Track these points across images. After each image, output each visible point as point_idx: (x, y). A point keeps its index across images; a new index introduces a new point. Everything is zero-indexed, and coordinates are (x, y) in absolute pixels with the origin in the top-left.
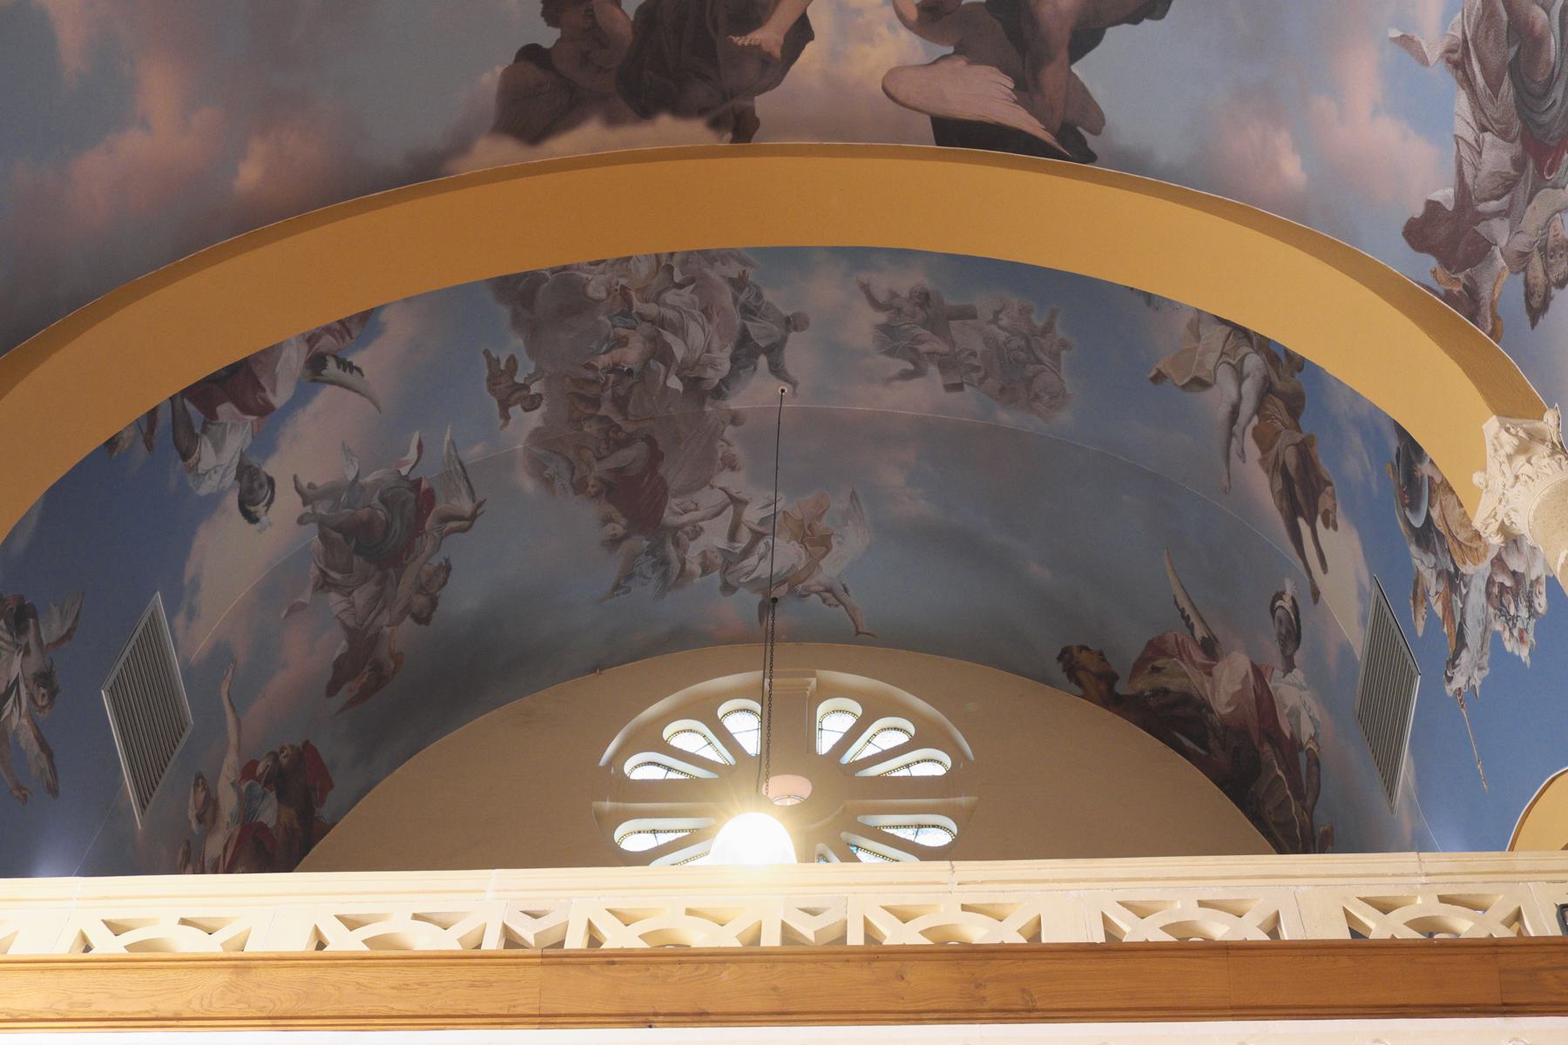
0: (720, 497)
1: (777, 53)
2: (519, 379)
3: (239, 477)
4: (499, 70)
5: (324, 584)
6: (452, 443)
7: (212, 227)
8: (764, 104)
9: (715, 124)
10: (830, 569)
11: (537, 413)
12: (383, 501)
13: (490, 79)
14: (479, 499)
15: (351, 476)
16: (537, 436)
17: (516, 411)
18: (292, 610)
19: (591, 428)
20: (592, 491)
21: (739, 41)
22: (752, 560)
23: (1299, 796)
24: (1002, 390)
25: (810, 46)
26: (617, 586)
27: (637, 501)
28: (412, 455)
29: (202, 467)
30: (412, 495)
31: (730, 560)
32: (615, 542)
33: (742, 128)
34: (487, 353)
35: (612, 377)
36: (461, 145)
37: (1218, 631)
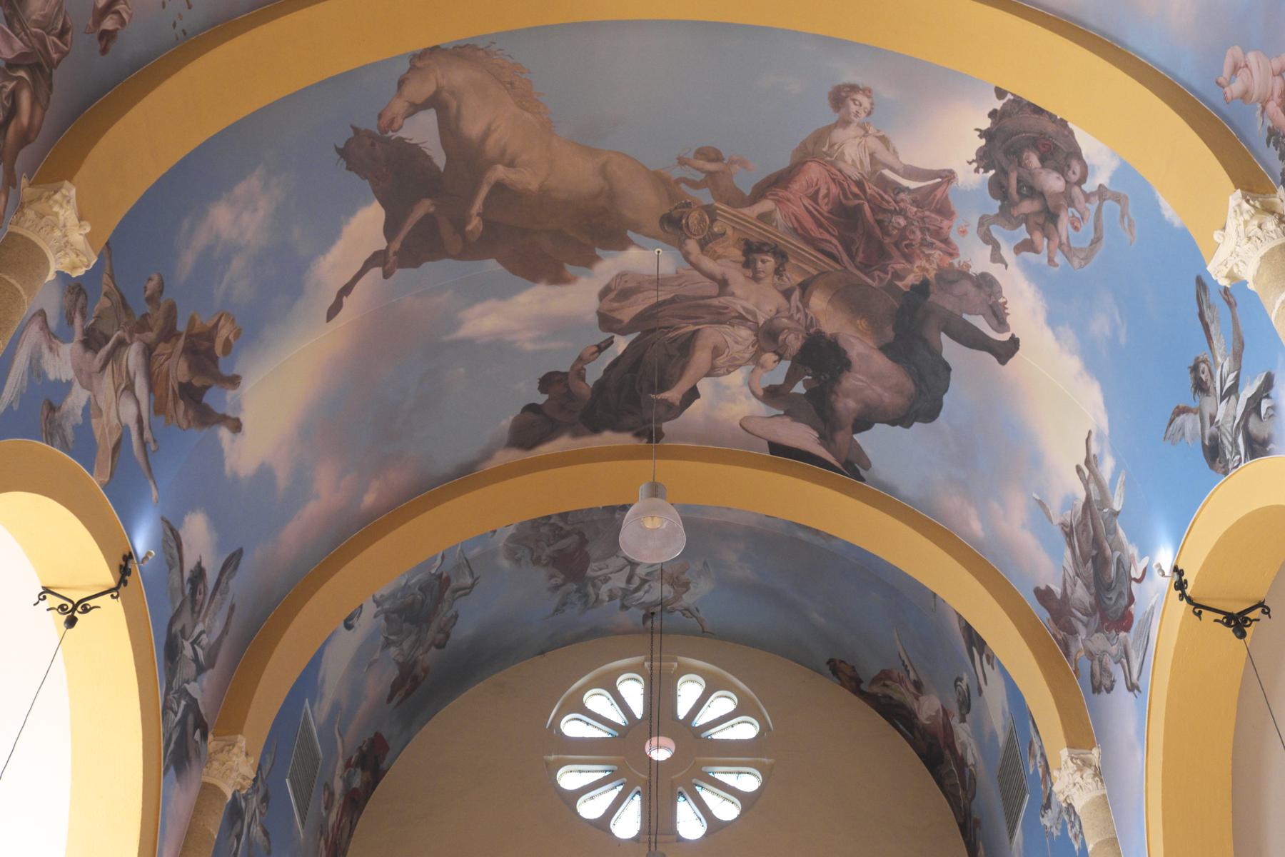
1: (678, 403)
4: (511, 418)
5: (388, 644)
8: (666, 427)
9: (638, 435)
10: (687, 600)
12: (420, 589)
13: (506, 423)
18: (369, 666)
22: (641, 593)
23: (964, 788)
25: (697, 402)
26: (557, 610)
31: (626, 593)
32: (557, 587)
33: (651, 435)
36: (488, 455)
37: (924, 681)
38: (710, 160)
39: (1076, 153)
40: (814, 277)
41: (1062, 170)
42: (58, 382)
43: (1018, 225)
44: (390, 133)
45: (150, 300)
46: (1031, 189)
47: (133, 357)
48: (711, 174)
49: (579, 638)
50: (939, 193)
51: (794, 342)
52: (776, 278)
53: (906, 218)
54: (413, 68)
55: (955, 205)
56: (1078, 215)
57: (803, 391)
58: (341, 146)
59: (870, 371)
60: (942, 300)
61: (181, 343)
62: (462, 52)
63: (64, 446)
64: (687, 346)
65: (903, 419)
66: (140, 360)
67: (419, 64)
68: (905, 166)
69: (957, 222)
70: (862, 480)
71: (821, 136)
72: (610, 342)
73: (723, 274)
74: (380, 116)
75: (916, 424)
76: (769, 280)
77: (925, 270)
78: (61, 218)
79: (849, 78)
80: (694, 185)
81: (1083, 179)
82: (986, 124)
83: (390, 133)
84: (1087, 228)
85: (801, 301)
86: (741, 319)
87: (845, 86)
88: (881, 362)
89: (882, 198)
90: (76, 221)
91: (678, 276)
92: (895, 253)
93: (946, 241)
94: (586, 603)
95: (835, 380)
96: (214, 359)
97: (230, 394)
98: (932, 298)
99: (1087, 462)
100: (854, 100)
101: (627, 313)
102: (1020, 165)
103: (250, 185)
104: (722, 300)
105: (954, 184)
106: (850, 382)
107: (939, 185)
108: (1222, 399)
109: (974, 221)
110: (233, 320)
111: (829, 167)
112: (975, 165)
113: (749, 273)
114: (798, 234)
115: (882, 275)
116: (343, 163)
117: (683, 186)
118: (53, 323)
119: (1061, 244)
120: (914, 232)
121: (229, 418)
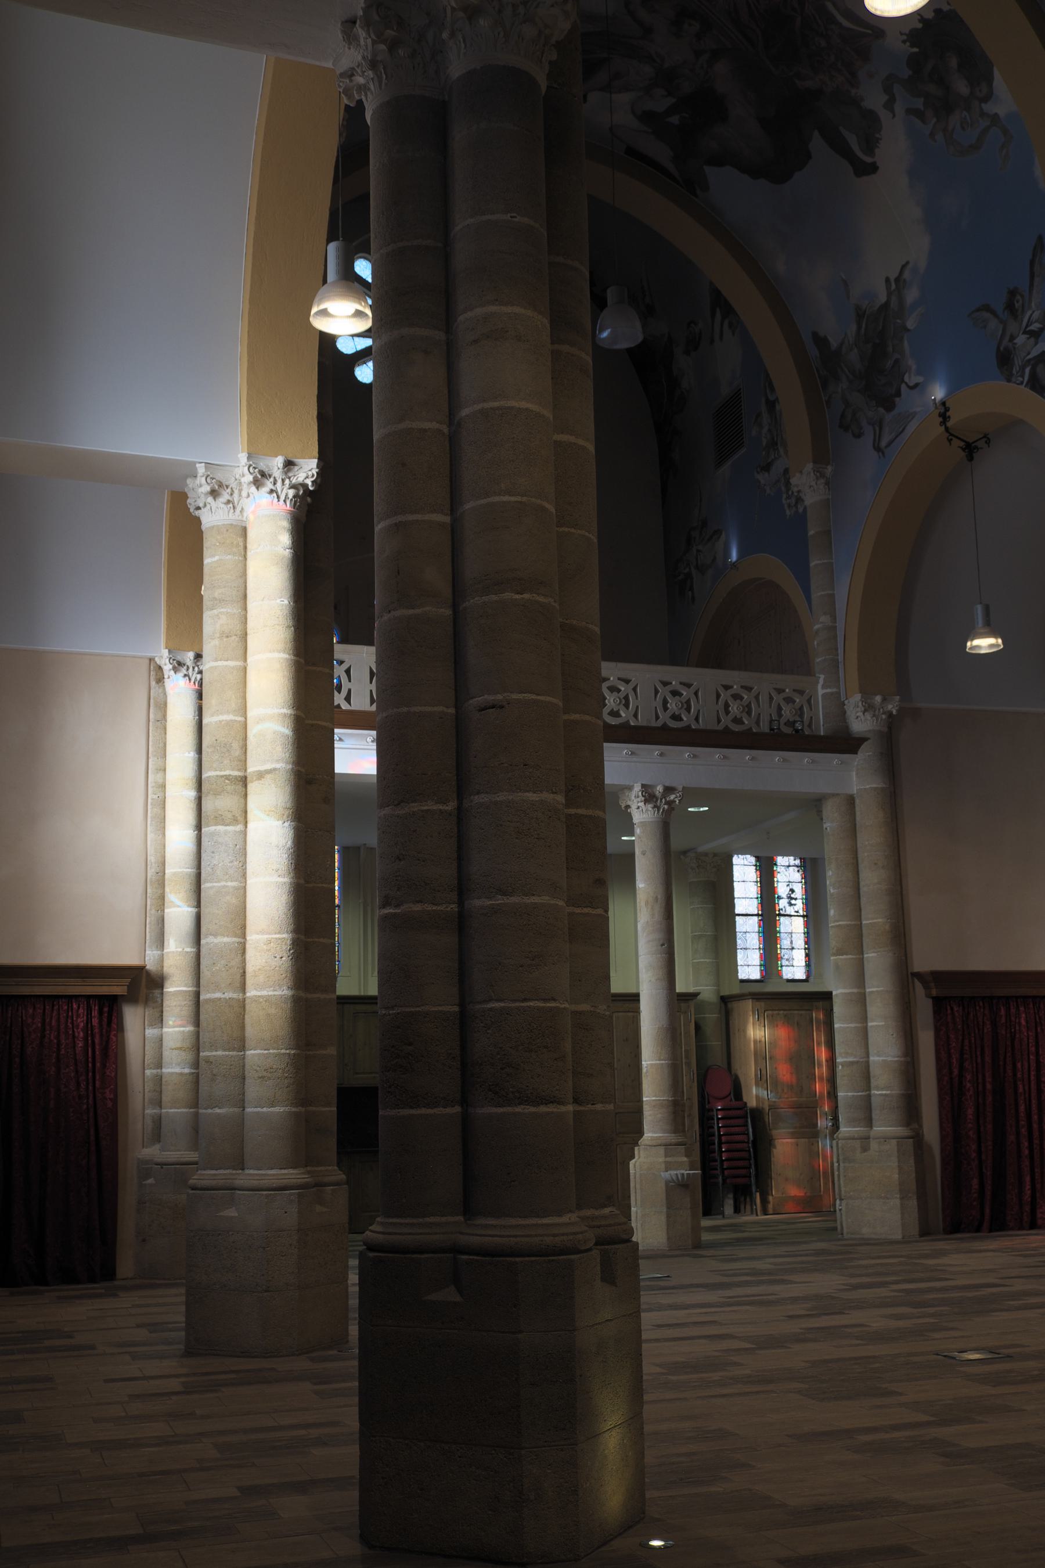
81: (986, 99)
99: (897, 280)
108: (1025, 332)
112: (905, 37)
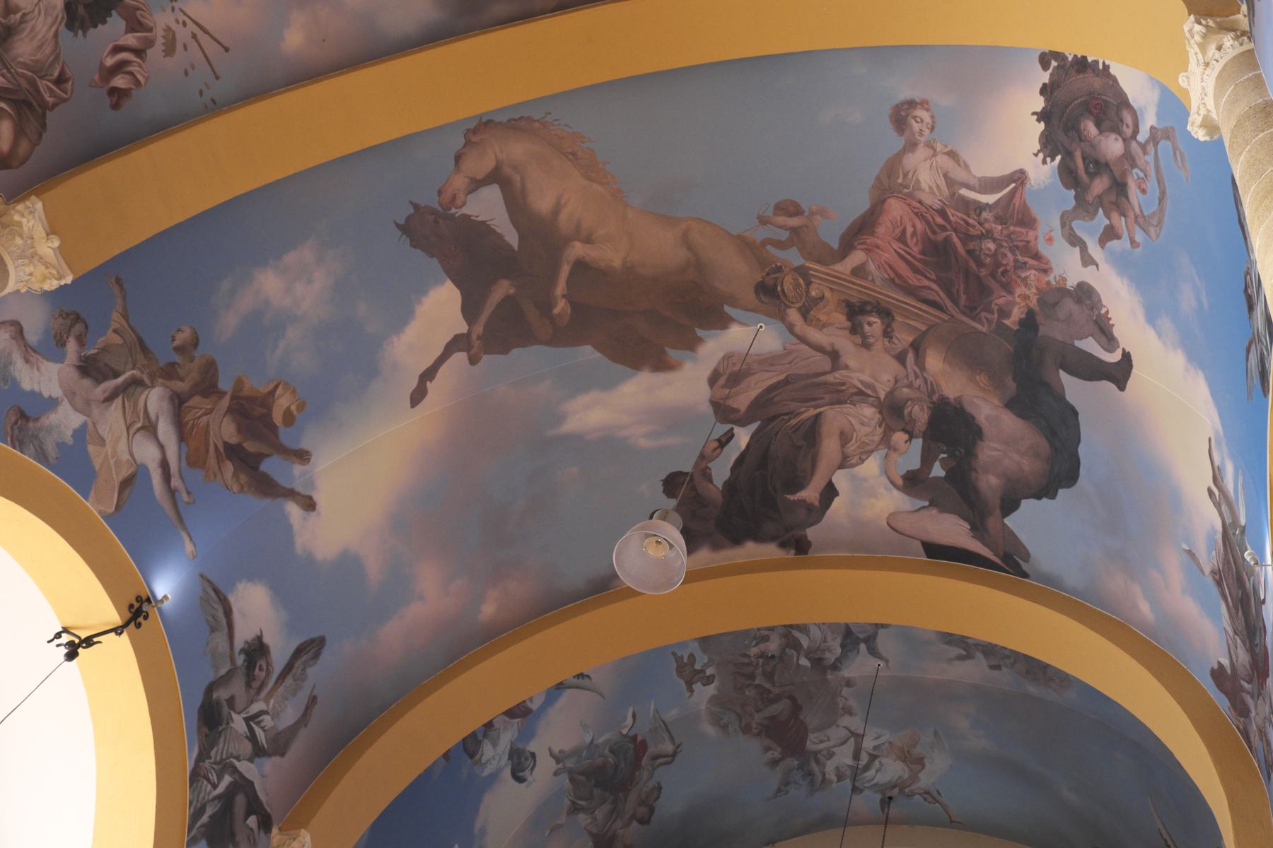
0: (844, 733)
1: (817, 503)
2: (698, 667)
3: (510, 757)
5: (575, 809)
6: (656, 711)
7: (464, 646)
8: (811, 533)
9: (783, 545)
10: (926, 780)
11: (712, 686)
12: (612, 751)
14: (678, 742)
15: (588, 739)
16: (714, 700)
17: (698, 687)
18: (552, 830)
19: (750, 693)
20: (755, 731)
21: (791, 497)
24: (1027, 672)
26: (779, 791)
27: (787, 736)
28: (629, 721)
29: (484, 759)
30: (632, 746)
31: (856, 773)
33: (801, 546)
34: (674, 654)
35: (761, 661)
38: (791, 215)
39: (1123, 102)
40: (924, 334)
41: (1116, 129)
42: (35, 396)
43: (1096, 212)
44: (453, 210)
45: (180, 350)
46: (1097, 162)
47: (155, 400)
48: (794, 230)
49: (807, 830)
50: (1017, 201)
51: (920, 414)
52: (886, 340)
53: (994, 240)
54: (468, 143)
55: (1036, 210)
56: (1141, 175)
57: (942, 473)
58: (402, 221)
59: (1005, 440)
60: (1051, 330)
61: (225, 402)
62: (516, 123)
63: (42, 456)
64: (812, 432)
65: (1046, 490)
66: (166, 405)
67: (474, 139)
68: (980, 179)
69: (1042, 230)
70: (1026, 575)
71: (893, 166)
72: (730, 436)
73: (832, 345)
74: (440, 193)
75: (1061, 492)
76: (879, 345)
77: (1026, 297)
78: (25, 229)
79: (905, 94)
80: (780, 245)
81: (1136, 131)
82: (1039, 104)
83: (453, 210)
84: (1152, 185)
85: (916, 364)
86: (861, 395)
87: (902, 104)
88: (1010, 423)
89: (967, 223)
90: (44, 234)
91: (787, 353)
92: (994, 285)
93: (1037, 256)
94: (812, 783)
95: (970, 454)
96: (273, 429)
97: (298, 469)
98: (1042, 331)
100: (915, 117)
101: (742, 401)
102: (1081, 140)
103: (304, 254)
104: (837, 374)
105: (1028, 186)
106: (989, 451)
107: (1014, 191)
109: (1056, 223)
110: (294, 392)
111: (909, 201)
113: (858, 340)
114: (896, 285)
115: (989, 316)
116: (406, 241)
117: (769, 247)
118: (32, 336)
119: (1136, 217)
120: (1005, 255)
121: (298, 494)
